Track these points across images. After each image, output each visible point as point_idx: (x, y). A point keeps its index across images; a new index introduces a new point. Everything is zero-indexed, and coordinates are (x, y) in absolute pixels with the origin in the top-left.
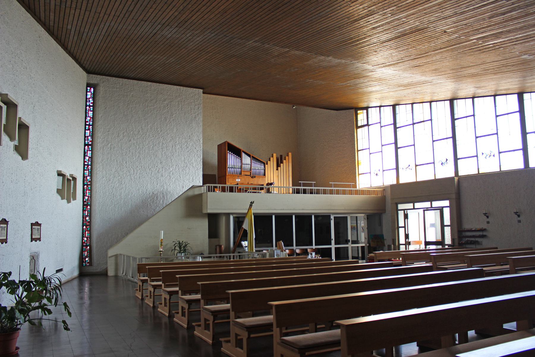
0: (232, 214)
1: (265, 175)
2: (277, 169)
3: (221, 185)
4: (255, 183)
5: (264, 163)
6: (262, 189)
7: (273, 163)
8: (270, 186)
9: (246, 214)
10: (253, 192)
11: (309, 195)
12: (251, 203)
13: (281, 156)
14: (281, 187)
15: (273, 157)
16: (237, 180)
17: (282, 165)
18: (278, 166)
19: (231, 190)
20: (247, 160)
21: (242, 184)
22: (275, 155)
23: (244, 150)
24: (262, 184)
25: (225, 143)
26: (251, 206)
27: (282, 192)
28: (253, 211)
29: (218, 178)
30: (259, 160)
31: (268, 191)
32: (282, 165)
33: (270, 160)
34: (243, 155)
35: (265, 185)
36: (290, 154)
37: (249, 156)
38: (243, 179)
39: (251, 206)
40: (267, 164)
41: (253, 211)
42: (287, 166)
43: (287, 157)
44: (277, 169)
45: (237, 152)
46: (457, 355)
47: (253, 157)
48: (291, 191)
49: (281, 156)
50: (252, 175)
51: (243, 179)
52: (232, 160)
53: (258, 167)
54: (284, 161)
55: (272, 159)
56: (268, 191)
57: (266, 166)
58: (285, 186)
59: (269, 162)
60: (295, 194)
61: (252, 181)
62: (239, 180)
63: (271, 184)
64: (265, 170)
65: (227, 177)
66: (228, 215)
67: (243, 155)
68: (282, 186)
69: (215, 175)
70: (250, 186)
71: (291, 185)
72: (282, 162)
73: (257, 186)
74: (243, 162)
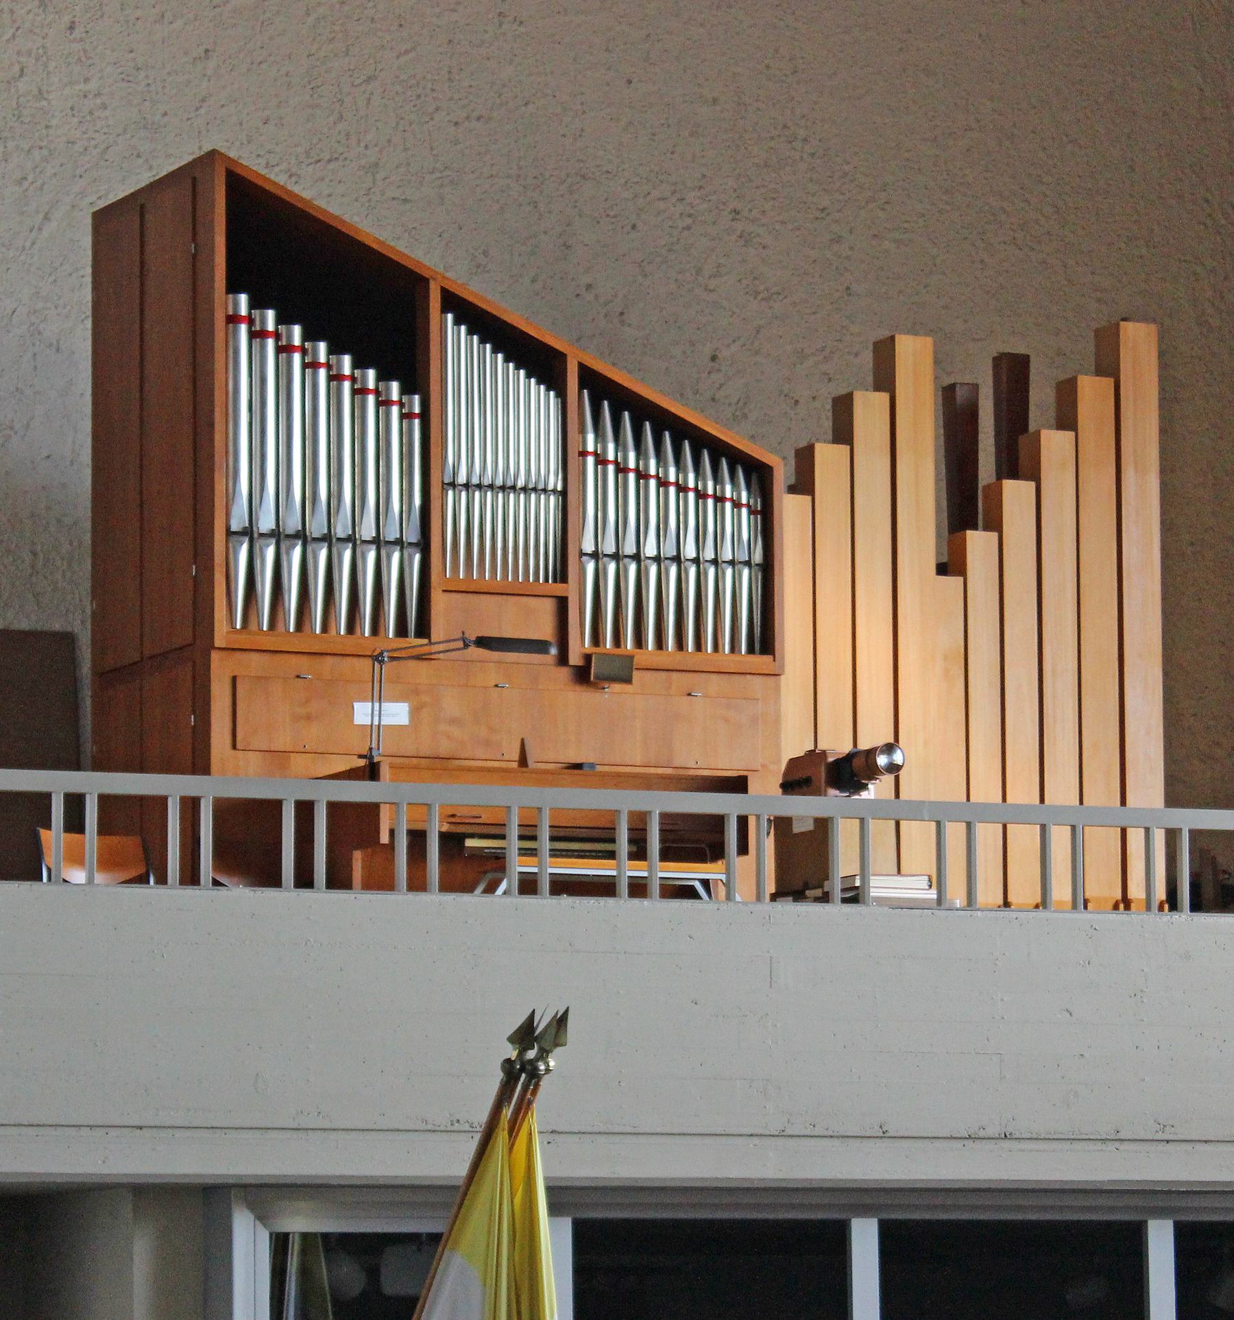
0: (263, 1195)
1: (765, 640)
2: (951, 564)
3: (95, 784)
4: (633, 753)
5: (758, 475)
6: (697, 840)
7: (888, 471)
8: (830, 802)
9: (455, 1197)
10: (564, 886)
11: (434, 901)
12: (525, 1035)
13: (1013, 373)
14: (1005, 817)
15: (885, 380)
16: (362, 713)
17: (1016, 493)
18: (966, 508)
19: (249, 845)
20: (503, 423)
21: (441, 765)
22: (913, 354)
23: (480, 291)
24: (727, 766)
25: (190, 178)
26: (520, 1078)
27: (1024, 889)
28: (553, 1151)
29: (106, 677)
30: (682, 431)
31: (804, 870)
32: (1016, 493)
33: (843, 433)
34: (457, 349)
35: (765, 795)
36: (1139, 343)
37: (541, 362)
38: (452, 703)
39: (520, 1078)
40: (804, 484)
41: (553, 1151)
42: (1095, 517)
43: (1092, 393)
44: (951, 564)
45: (368, 311)
46: (667, 433)
47: (589, 378)
48: (1148, 874)
49: (1013, 373)
50: (581, 643)
51: (452, 703)
52: (290, 429)
53: (668, 524)
54: (1054, 445)
55: (869, 410)
56: (804, 870)
57: (790, 508)
58: (1062, 791)
59: (828, 457)
60: (1184, 918)
61: (576, 723)
62: (397, 713)
63: (850, 772)
64: (767, 571)
65: (220, 670)
66: (196, 1210)
67: (457, 349)
68: (986, 790)
69: (67, 640)
70: (514, 800)
71: (1149, 787)
72: (1019, 460)
73: (624, 802)
74: (458, 457)
